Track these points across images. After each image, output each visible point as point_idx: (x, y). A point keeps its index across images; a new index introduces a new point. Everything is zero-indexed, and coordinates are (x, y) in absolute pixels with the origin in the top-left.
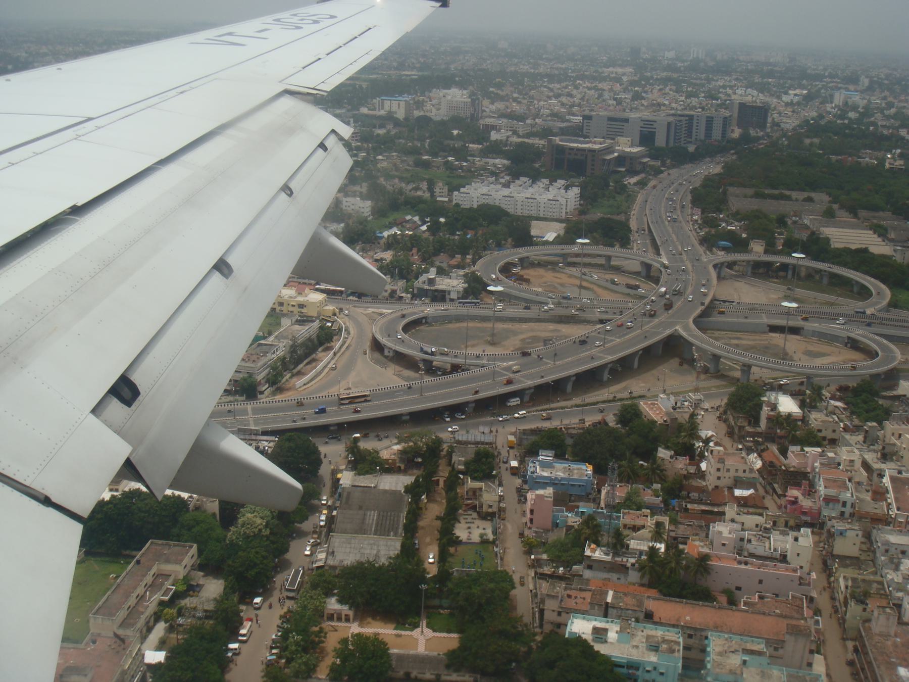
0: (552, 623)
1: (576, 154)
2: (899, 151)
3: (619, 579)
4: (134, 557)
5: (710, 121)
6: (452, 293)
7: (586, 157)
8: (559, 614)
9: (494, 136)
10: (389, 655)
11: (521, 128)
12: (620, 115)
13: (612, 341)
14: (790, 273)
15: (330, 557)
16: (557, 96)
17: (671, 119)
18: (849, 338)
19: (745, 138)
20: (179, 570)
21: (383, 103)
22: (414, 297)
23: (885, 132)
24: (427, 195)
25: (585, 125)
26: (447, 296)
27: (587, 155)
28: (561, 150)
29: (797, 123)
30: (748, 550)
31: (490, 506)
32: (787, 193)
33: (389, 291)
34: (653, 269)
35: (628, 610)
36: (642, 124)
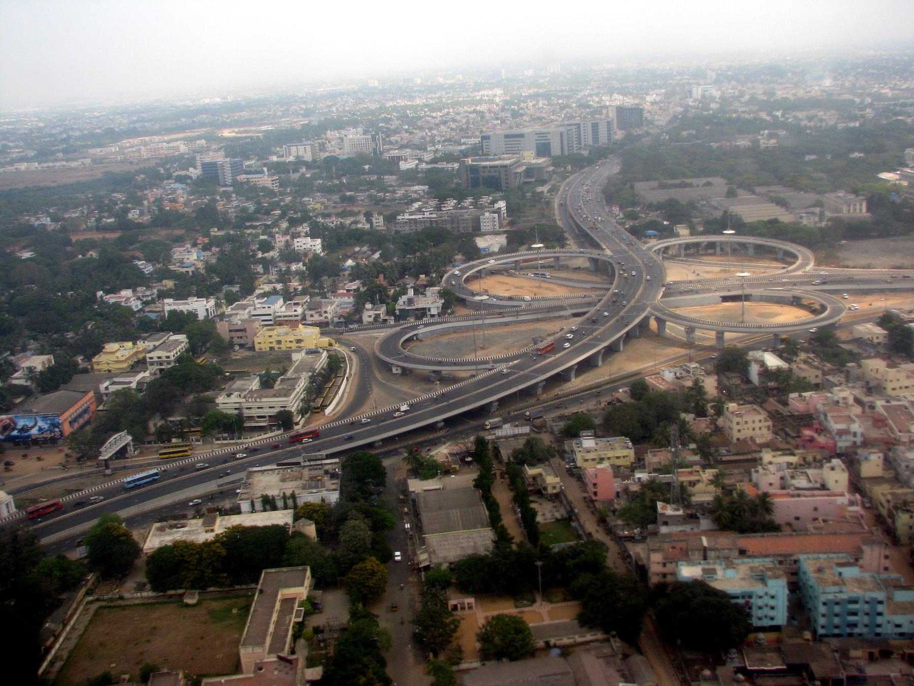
0: (658, 575)
1: (490, 172)
2: (766, 132)
3: (692, 529)
4: (256, 589)
5: (595, 127)
6: (432, 310)
7: (500, 174)
8: (664, 565)
9: (404, 166)
10: (528, 629)
11: (428, 157)
12: (515, 131)
13: (599, 329)
14: (718, 249)
15: (433, 556)
16: (445, 123)
17: (562, 129)
18: (794, 297)
19: (629, 138)
20: (302, 592)
21: (289, 150)
22: (398, 319)
23: (747, 116)
24: (367, 226)
25: (484, 144)
26: (428, 313)
27: (499, 171)
28: (474, 170)
29: (668, 118)
30: (793, 485)
31: (554, 488)
32: (688, 181)
33: (373, 316)
34: (599, 263)
35: (724, 549)
36: (536, 137)
